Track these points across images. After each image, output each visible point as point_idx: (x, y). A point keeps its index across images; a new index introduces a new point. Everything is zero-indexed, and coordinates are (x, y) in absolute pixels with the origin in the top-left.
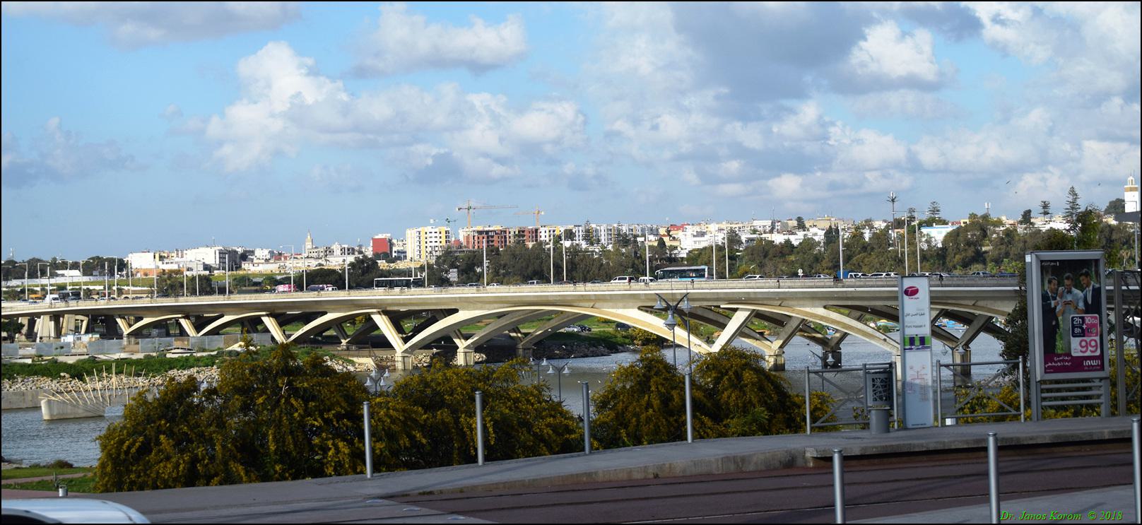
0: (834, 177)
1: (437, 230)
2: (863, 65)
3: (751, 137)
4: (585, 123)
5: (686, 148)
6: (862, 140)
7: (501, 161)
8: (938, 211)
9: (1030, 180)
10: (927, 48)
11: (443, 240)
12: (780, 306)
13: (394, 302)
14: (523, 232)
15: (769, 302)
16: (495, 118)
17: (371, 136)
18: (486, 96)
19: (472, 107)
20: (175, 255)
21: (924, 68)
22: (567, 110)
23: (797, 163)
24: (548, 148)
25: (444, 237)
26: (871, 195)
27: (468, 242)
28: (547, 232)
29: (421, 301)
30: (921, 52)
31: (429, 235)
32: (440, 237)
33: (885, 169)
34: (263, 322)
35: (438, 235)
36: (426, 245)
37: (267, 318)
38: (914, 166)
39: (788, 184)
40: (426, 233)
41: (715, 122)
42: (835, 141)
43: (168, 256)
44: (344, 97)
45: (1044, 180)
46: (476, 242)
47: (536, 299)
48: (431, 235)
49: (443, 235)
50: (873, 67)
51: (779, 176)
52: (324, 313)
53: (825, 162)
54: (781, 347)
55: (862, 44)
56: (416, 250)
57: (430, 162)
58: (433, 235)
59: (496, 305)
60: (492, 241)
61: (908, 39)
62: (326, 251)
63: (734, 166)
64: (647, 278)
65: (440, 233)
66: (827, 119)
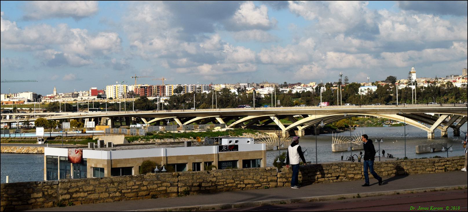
0: (225, 66)
1: (122, 86)
2: (239, 20)
3: (190, 48)
4: (121, 41)
5: (164, 53)
6: (237, 50)
7: (84, 57)
8: (348, 80)
9: (305, 68)
10: (265, 13)
11: (125, 90)
12: (461, 113)
13: (283, 112)
14: (159, 87)
15: (456, 112)
16: (83, 39)
17: (28, 46)
18: (78, 30)
19: (73, 34)
20: (13, 95)
21: (264, 21)
22: (113, 36)
23: (210, 60)
24: (105, 52)
25: (125, 89)
26: (241, 73)
27: (136, 91)
28: (168, 87)
29: (297, 112)
30: (263, 15)
31: (119, 88)
32: (124, 89)
33: (246, 62)
34: (216, 119)
35: (123, 88)
36: (118, 92)
37: (176, 119)
38: (258, 61)
39: (205, 68)
40: (118, 87)
41: (177, 42)
42: (227, 51)
43: (10, 96)
44: (16, 29)
45: (311, 68)
46: (140, 91)
47: (352, 111)
48: (120, 88)
49: (125, 88)
50: (243, 21)
51: (202, 65)
52: (195, 117)
53: (222, 59)
54: (447, 129)
55: (239, 11)
56: (113, 93)
57: (54, 57)
58: (121, 88)
59: (330, 113)
60: (146, 91)
61: (258, 10)
62: (72, 95)
63: (184, 60)
64: (194, 108)
65: (124, 87)
66: (223, 41)
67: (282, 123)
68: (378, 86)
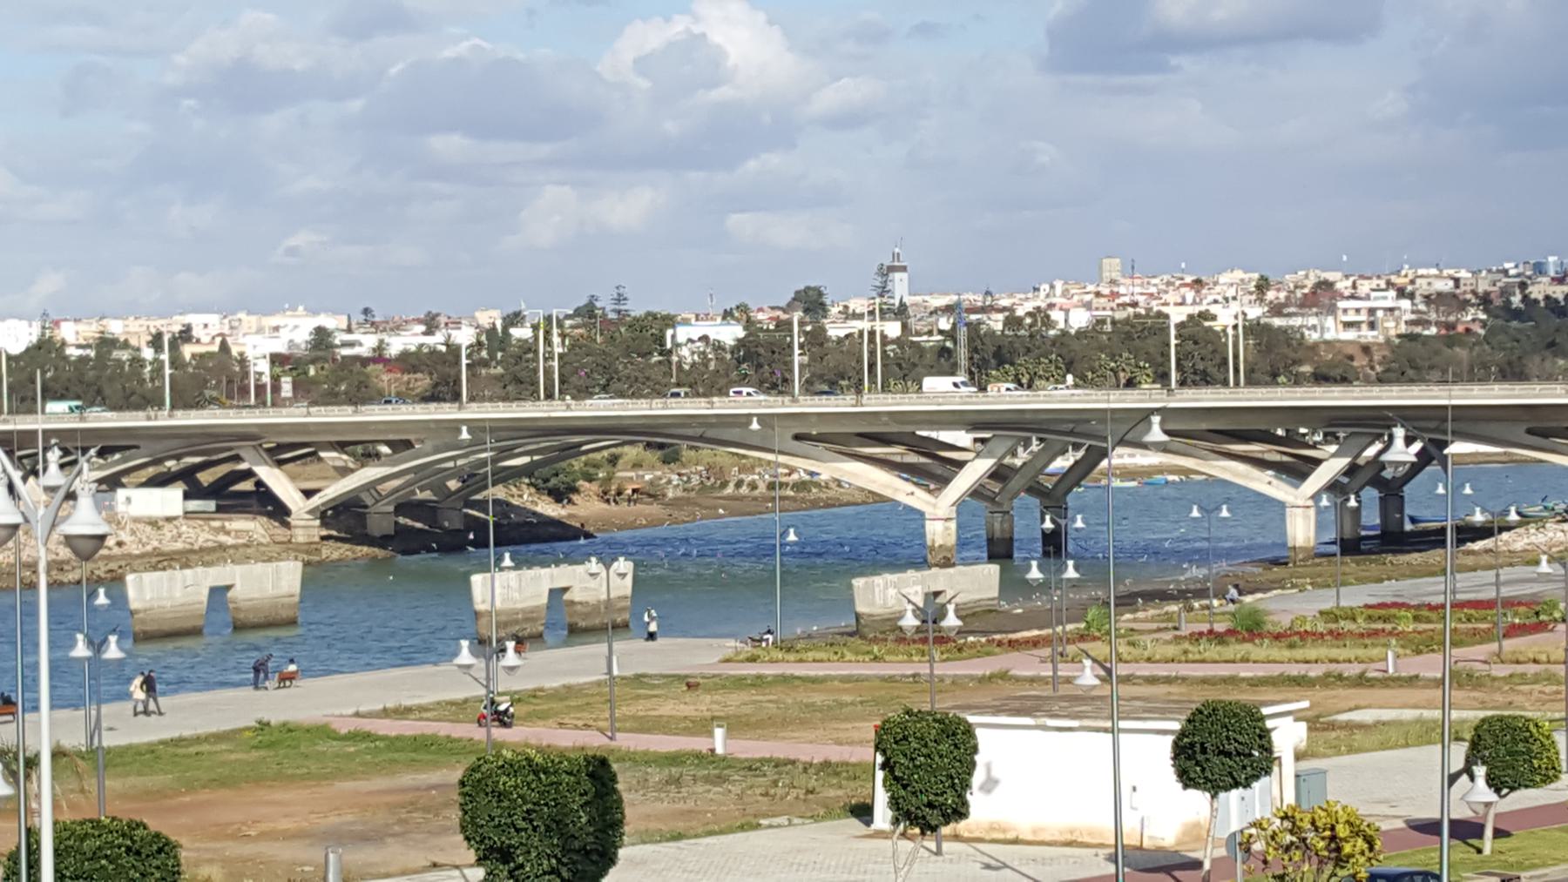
8: (625, 299)
47: (643, 425)
67: (293, 478)
68: (749, 324)
